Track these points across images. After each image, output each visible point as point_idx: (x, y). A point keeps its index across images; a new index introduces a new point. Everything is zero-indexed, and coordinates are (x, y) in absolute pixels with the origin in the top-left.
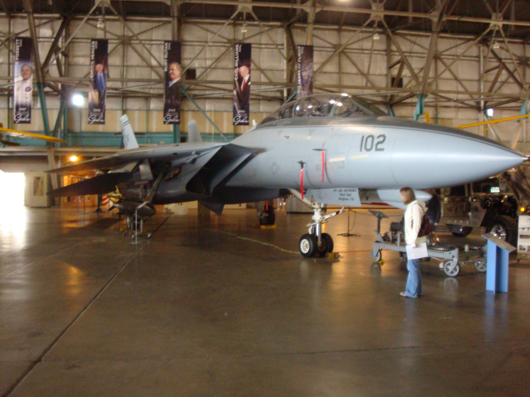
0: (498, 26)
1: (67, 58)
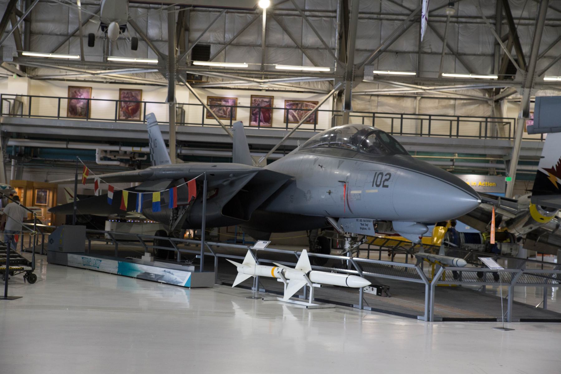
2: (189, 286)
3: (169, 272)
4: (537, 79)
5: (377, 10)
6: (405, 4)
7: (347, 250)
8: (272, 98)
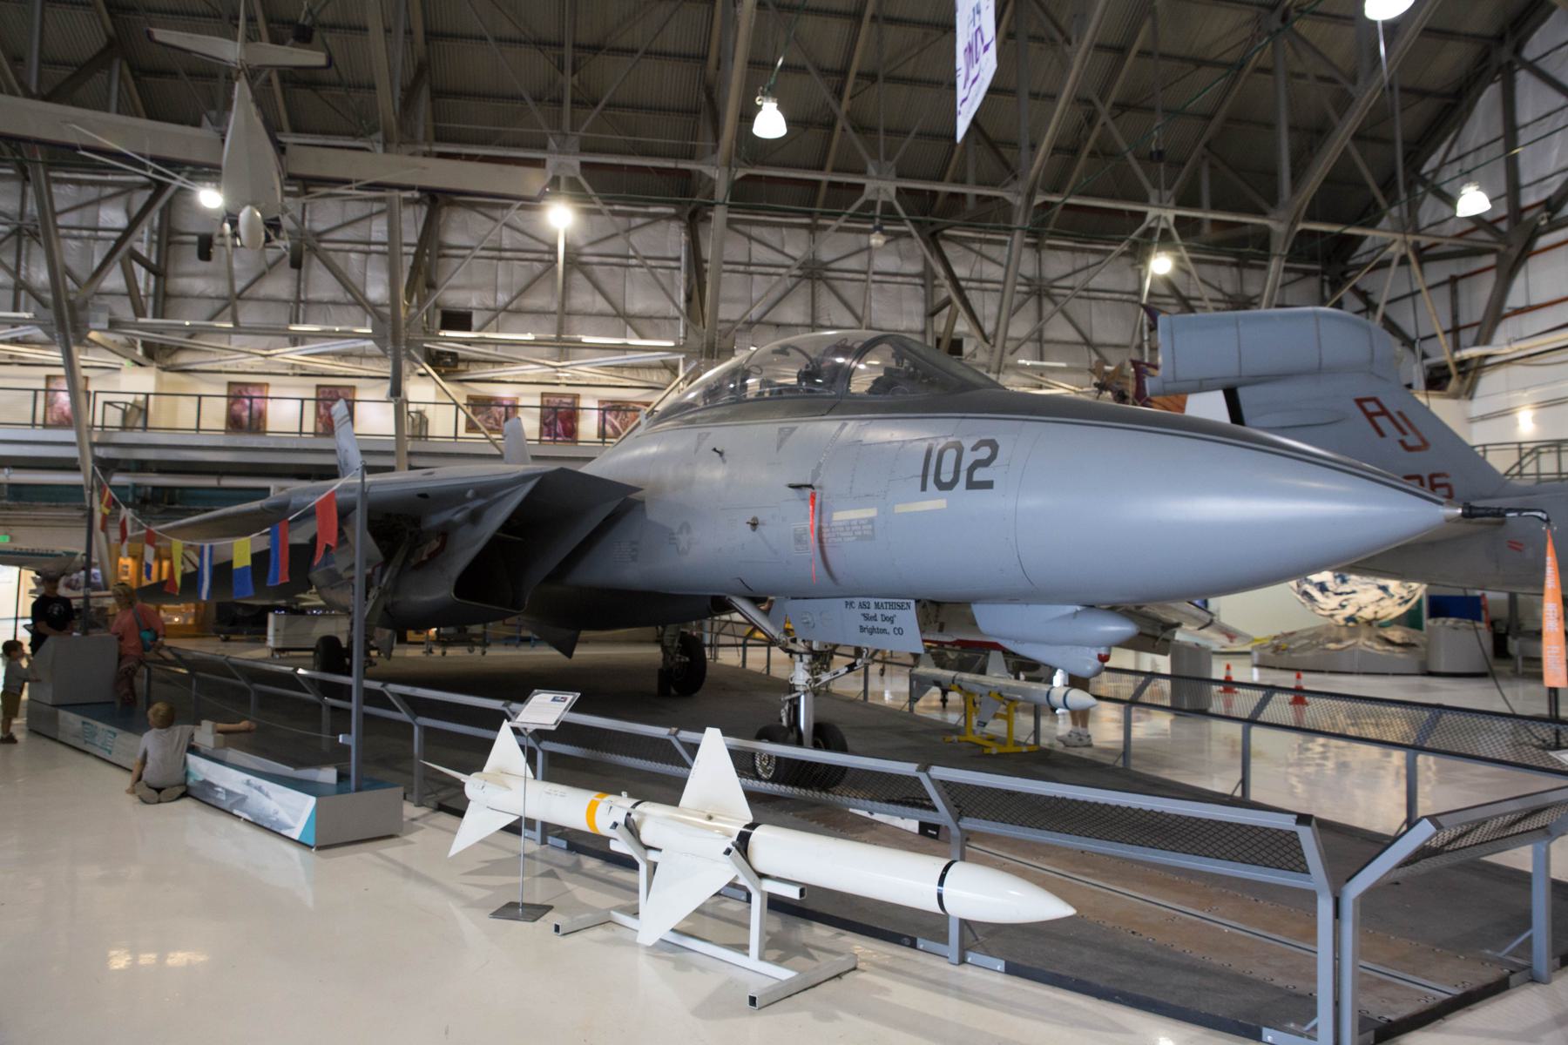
0: (1166, 219)
1: (161, 280)
2: (311, 842)
3: (259, 789)
4: (1008, 359)
5: (745, 259)
6: (787, 250)
7: (802, 689)
8: (577, 397)
